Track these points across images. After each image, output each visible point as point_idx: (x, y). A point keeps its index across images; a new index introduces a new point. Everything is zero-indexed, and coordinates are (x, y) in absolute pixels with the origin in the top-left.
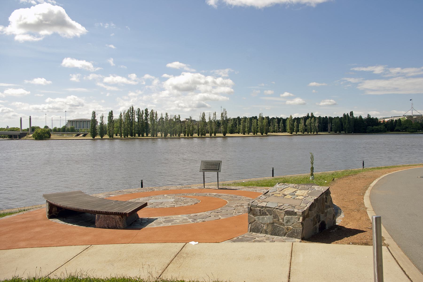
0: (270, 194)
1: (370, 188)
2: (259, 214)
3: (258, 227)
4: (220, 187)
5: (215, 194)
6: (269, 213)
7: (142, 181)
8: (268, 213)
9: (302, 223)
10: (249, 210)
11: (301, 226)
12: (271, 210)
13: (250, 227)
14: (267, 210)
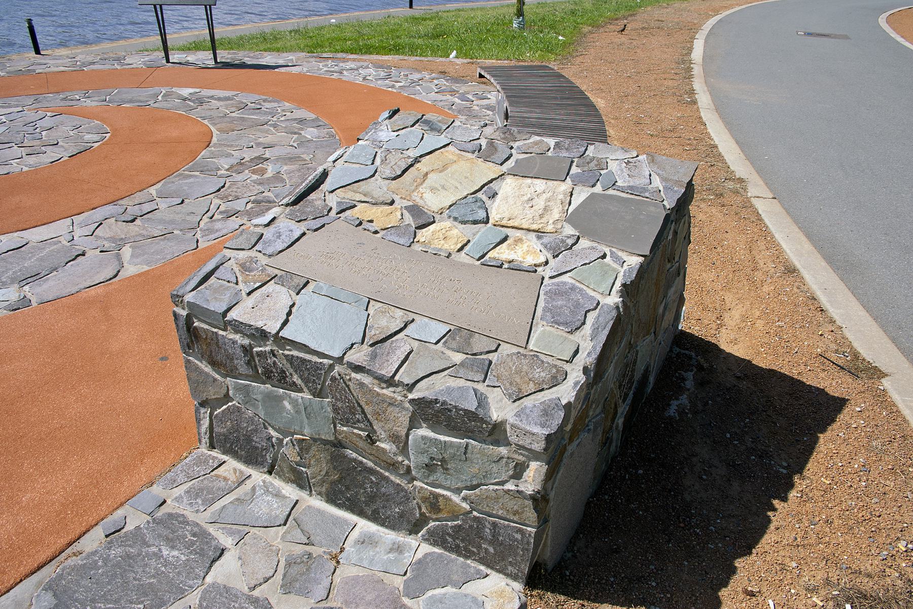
0: (333, 201)
1: (697, 70)
2: (243, 369)
3: (249, 439)
4: (224, 55)
5: (186, 92)
6: (306, 381)
7: (30, 21)
8: (296, 378)
9: (539, 500)
10: (185, 335)
11: (531, 515)
12: (317, 367)
13: (206, 423)
14: (290, 359)
